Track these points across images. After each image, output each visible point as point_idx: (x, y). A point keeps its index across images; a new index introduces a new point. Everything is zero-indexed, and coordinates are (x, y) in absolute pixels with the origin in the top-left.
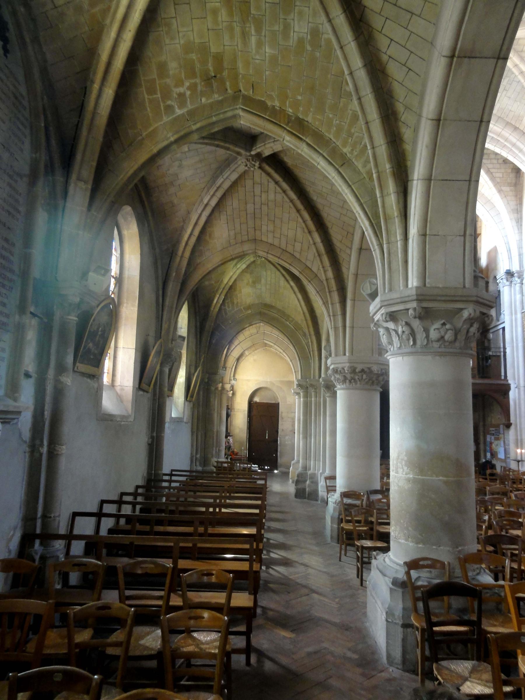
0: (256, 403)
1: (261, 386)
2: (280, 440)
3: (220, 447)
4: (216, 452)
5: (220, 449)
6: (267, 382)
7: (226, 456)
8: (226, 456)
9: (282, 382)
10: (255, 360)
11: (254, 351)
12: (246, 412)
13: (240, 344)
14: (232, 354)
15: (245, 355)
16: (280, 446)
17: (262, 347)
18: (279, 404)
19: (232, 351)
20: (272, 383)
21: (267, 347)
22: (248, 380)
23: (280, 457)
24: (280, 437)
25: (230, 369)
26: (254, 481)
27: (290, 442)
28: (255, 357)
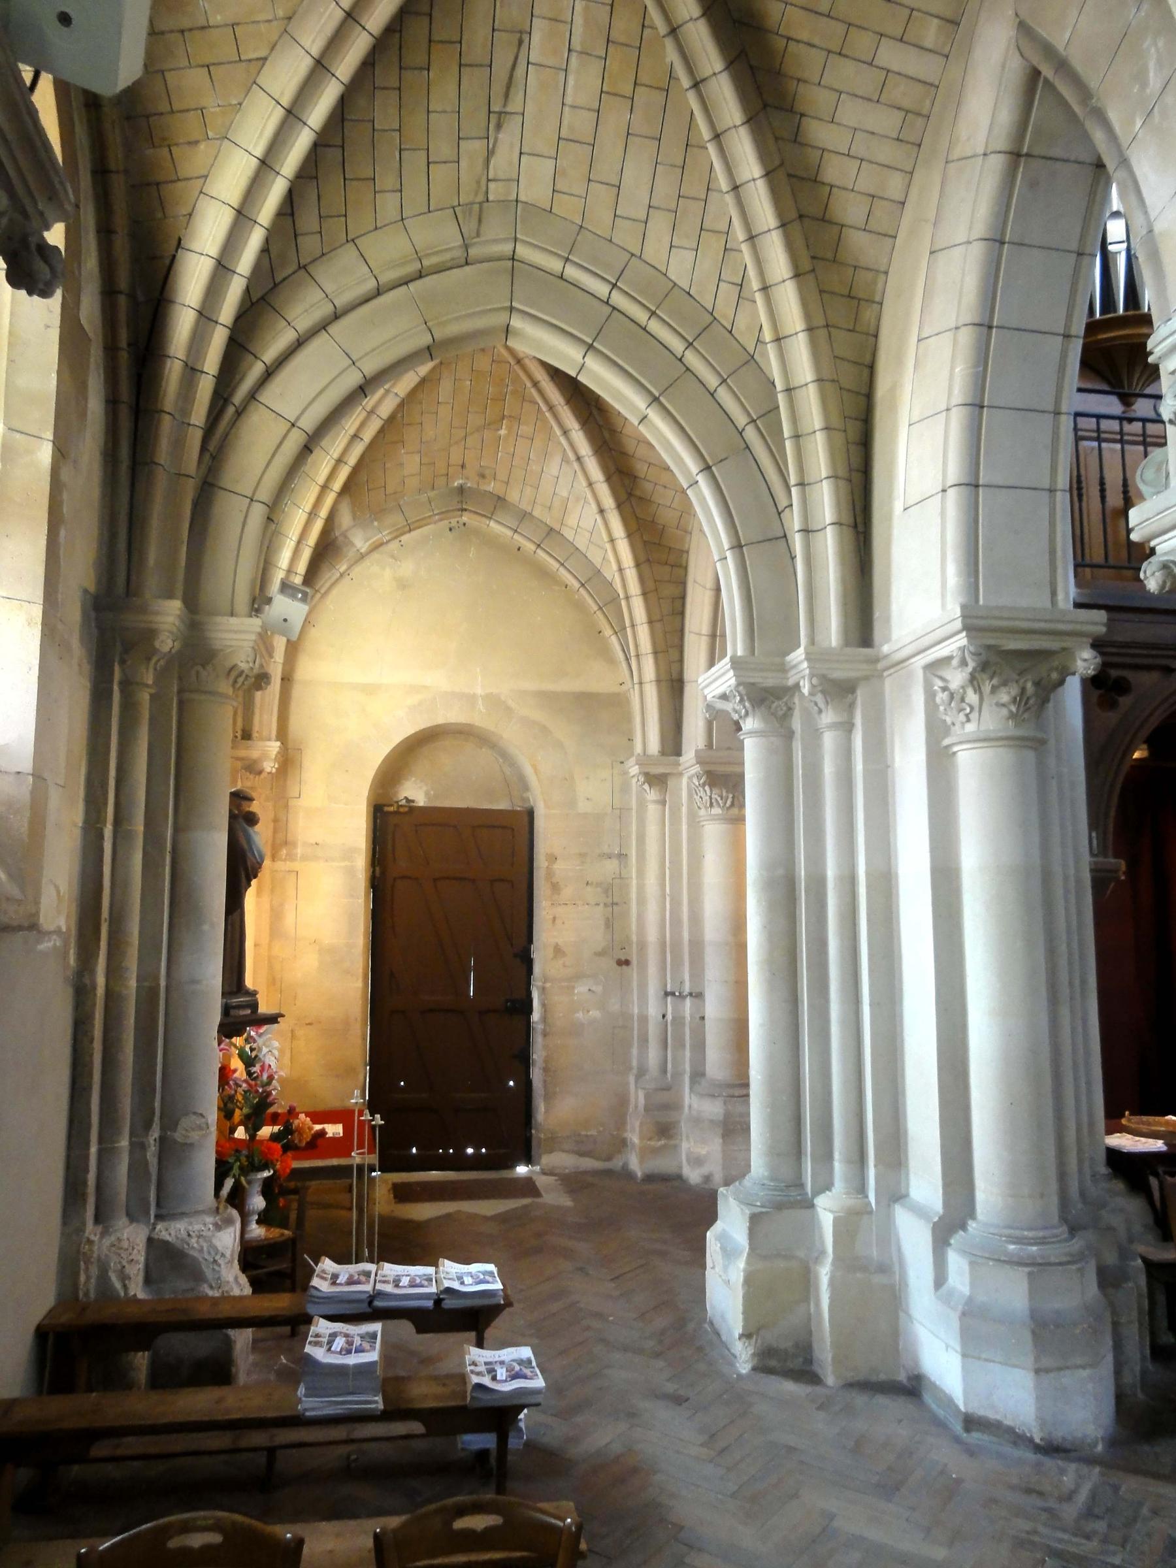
0: (412, 809)
1: (440, 720)
2: (543, 1005)
3: (170, 1122)
4: (138, 1169)
5: (178, 1136)
6: (471, 699)
7: (229, 1183)
8: (229, 1183)
9: (548, 699)
10: (402, 585)
11: (398, 534)
12: (361, 862)
13: (334, 329)
14: (268, 396)
15: (351, 554)
16: (545, 1034)
17: (444, 515)
18: (531, 814)
19: (269, 374)
20: (493, 701)
21: (465, 518)
22: (370, 690)
23: (548, 1097)
24: (543, 990)
25: (258, 512)
26: (180, 587)
27: (595, 1014)
28: (407, 568)
